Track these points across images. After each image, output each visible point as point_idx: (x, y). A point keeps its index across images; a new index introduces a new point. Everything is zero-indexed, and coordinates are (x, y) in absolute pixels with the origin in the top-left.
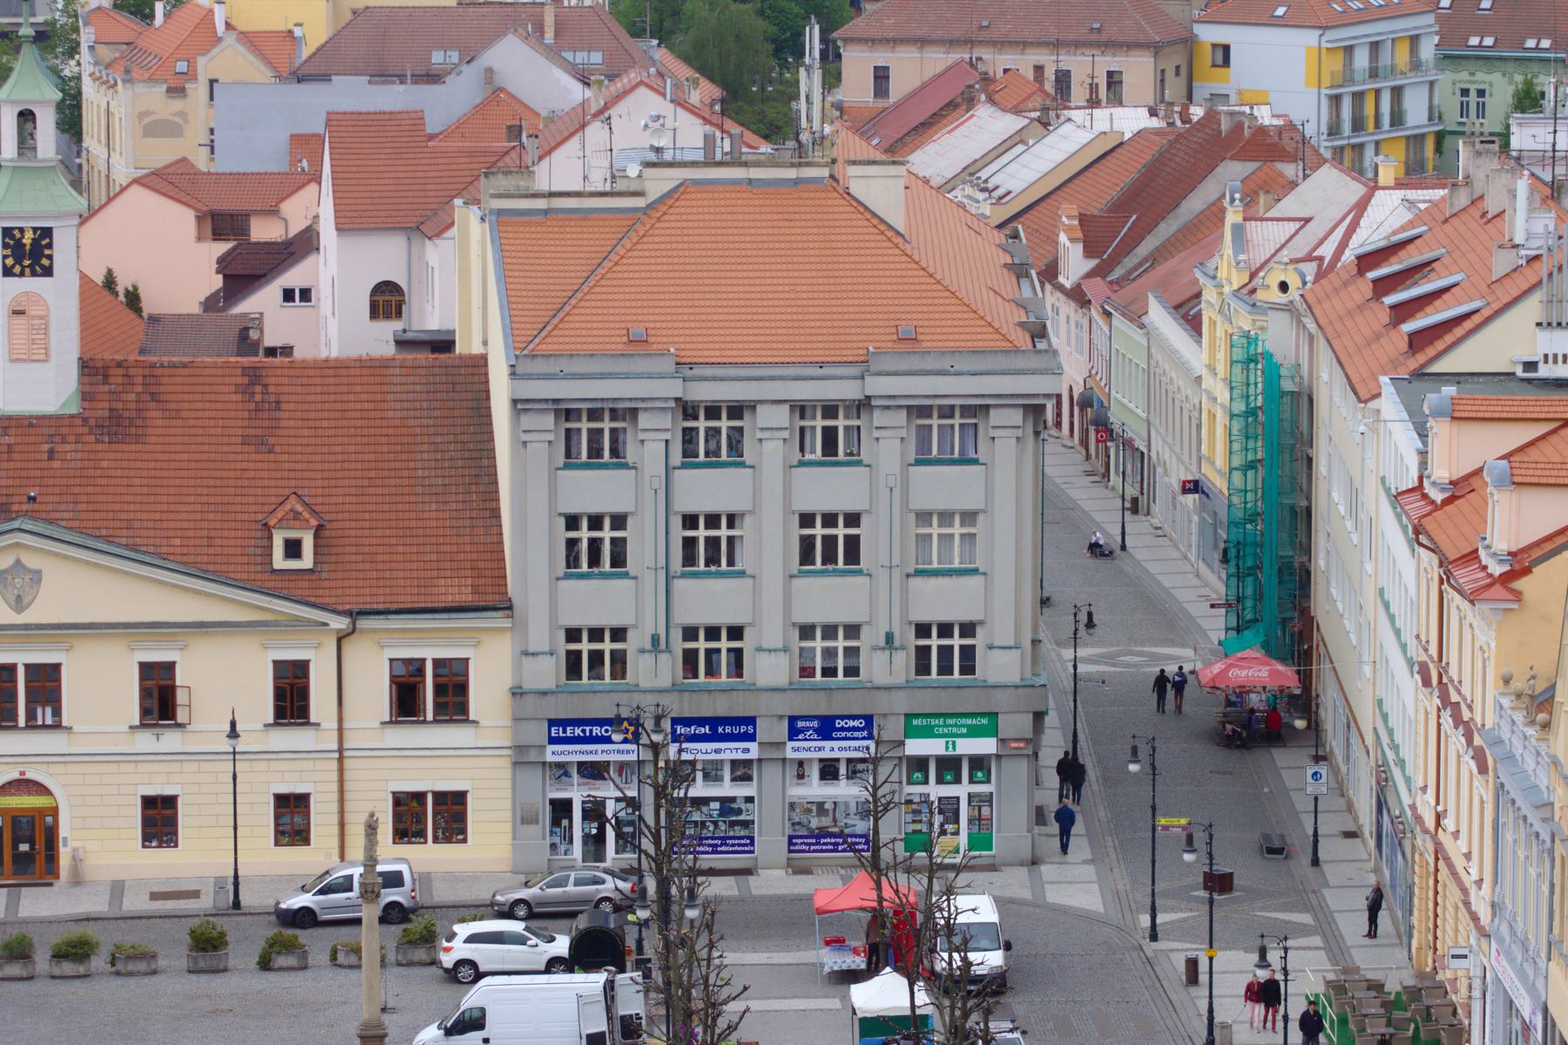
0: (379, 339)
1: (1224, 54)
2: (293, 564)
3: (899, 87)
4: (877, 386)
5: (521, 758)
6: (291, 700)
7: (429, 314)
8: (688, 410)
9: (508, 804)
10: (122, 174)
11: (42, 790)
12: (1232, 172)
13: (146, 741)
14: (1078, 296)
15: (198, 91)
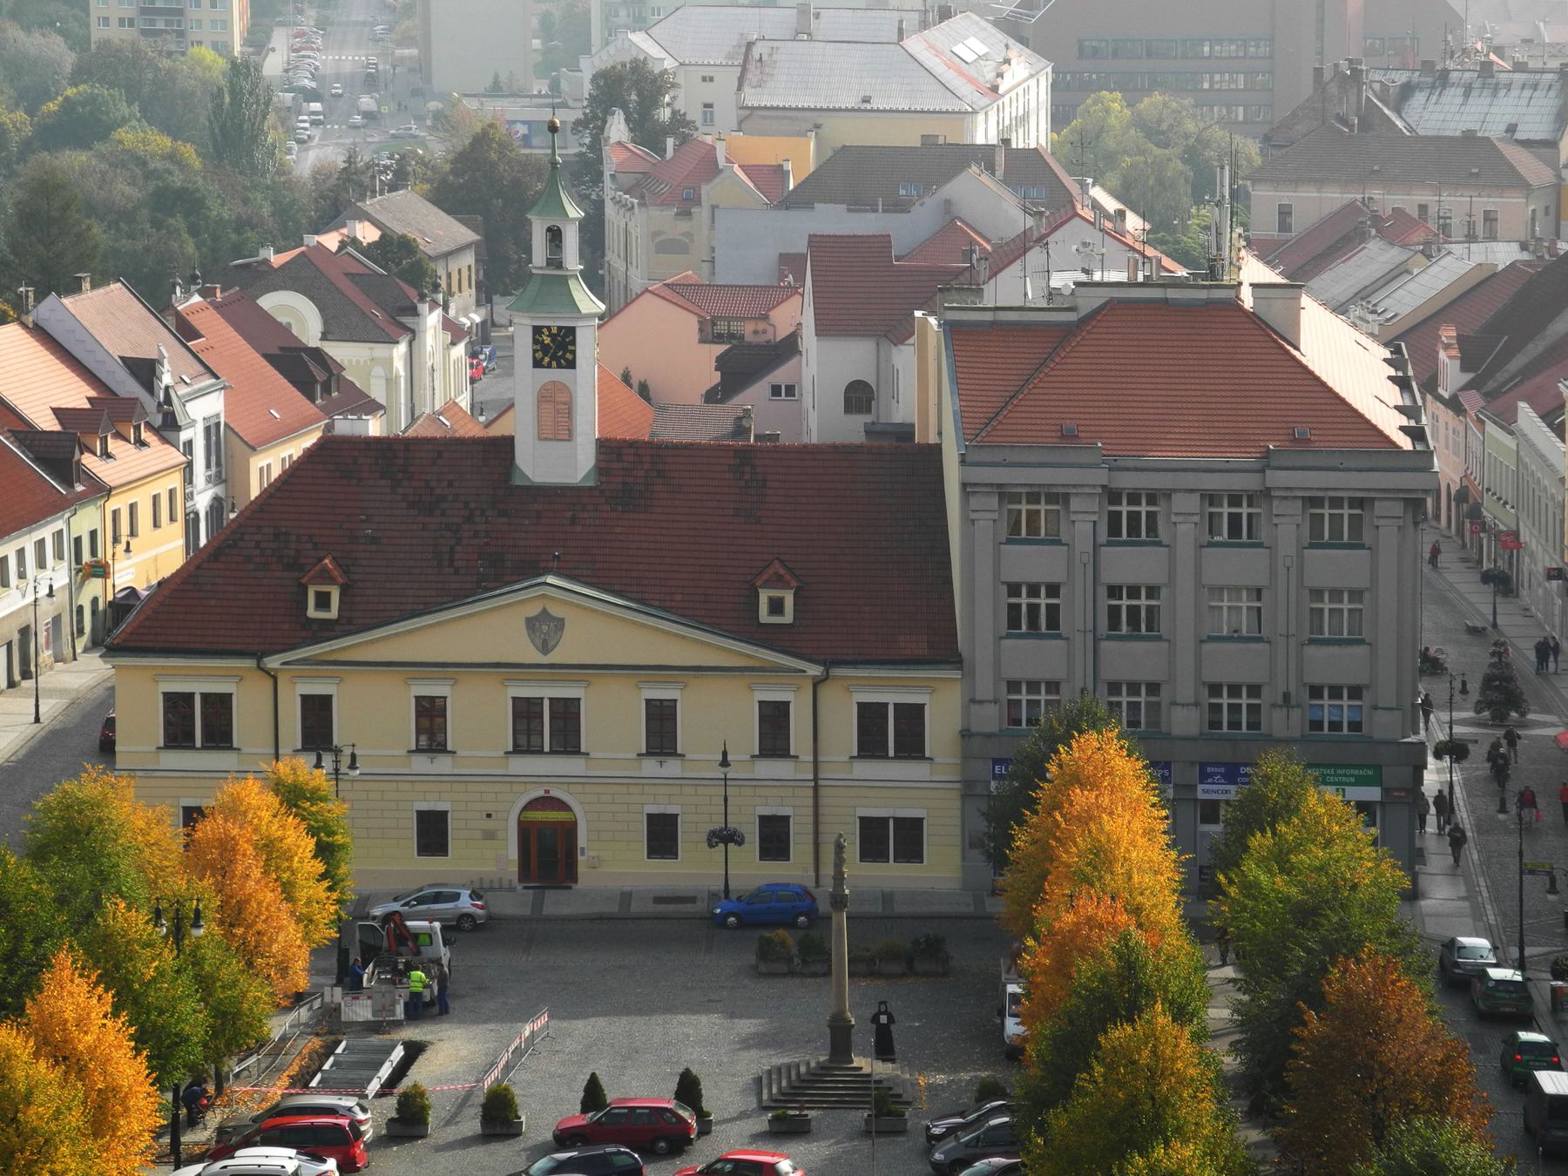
0: (852, 430)
3: (1299, 223)
4: (1277, 478)
6: (774, 719)
7: (903, 407)
8: (1114, 496)
9: (958, 831)
10: (637, 281)
11: (562, 805)
14: (1454, 405)
15: (702, 214)
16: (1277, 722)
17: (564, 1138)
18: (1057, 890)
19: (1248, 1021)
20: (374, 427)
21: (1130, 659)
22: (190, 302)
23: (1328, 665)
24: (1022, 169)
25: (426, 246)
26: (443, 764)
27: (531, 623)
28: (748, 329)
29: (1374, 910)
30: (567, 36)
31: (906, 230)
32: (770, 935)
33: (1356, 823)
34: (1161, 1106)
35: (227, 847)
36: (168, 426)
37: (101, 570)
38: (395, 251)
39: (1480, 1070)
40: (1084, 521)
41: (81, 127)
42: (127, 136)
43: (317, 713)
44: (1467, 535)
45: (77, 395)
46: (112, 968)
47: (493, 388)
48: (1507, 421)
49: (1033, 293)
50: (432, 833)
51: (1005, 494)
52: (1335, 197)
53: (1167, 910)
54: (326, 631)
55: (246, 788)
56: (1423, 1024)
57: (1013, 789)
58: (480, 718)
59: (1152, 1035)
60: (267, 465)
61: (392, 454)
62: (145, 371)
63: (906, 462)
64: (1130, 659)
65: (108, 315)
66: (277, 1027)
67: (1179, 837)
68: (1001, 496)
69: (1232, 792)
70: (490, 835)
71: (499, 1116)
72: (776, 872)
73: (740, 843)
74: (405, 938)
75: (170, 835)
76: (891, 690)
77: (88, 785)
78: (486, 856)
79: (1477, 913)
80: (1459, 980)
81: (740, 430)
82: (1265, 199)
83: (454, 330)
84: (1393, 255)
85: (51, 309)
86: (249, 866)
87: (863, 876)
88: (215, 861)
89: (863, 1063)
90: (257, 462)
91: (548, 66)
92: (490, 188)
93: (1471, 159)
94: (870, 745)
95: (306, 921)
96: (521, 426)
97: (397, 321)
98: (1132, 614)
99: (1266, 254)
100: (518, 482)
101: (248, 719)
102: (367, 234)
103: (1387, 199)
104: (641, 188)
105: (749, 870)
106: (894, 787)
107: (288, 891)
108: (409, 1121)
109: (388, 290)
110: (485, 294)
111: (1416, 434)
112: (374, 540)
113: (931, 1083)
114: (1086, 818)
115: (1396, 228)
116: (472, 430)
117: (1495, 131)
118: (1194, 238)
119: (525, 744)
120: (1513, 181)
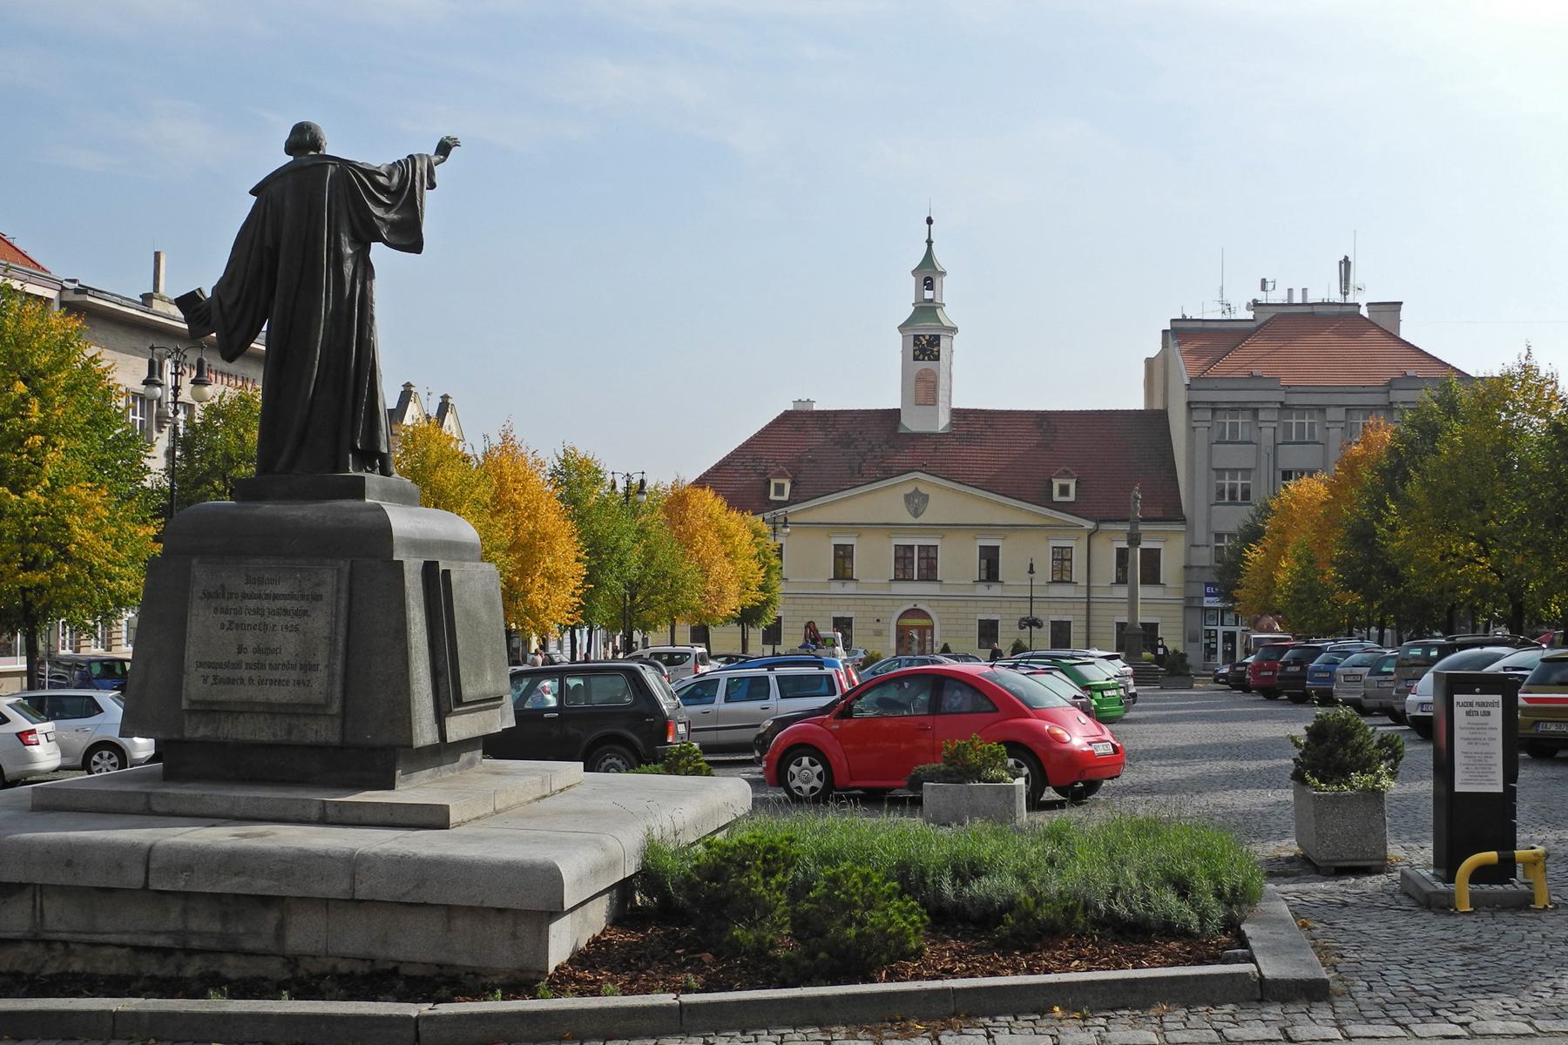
2: (1065, 482)
5: (1190, 604)
6: (1062, 558)
8: (1284, 407)
9: (1181, 631)
11: (925, 615)
13: (982, 590)
26: (850, 588)
27: (908, 498)
51: (1215, 408)
68: (1214, 410)
70: (878, 633)
73: (1040, 626)
100: (901, 431)
112: (811, 461)
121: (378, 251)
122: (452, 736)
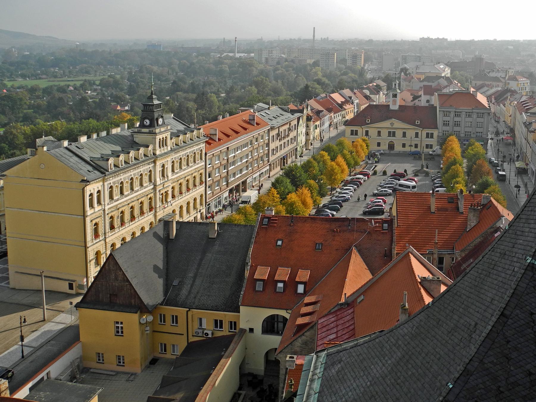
0: (427, 105)
1: (509, 83)
3: (477, 85)
4: (474, 111)
6: (417, 135)
7: (433, 102)
8: (456, 112)
10: (404, 89)
12: (509, 94)
13: (378, 137)
14: (494, 104)
15: (411, 83)
16: (472, 136)
17: (392, 176)
18: (447, 152)
19: (467, 166)
20: (375, 103)
21: (456, 129)
22: (355, 91)
23: (479, 130)
24: (447, 79)
25: (381, 85)
26: (380, 137)
28: (416, 94)
29: (482, 155)
30: (398, 65)
31: (434, 85)
32: (416, 156)
33: (481, 146)
34: (457, 174)
35: (357, 145)
36: (353, 103)
37: (345, 117)
38: (378, 86)
39: (492, 171)
40: (452, 114)
41: (345, 74)
42: (350, 75)
43: (367, 132)
44: (188, 197)
45: (343, 100)
46: (344, 157)
47: (387, 100)
48: (499, 106)
49: (448, 91)
50: (379, 144)
51: (444, 111)
52: (481, 82)
53: (459, 154)
54: (368, 124)
55: (359, 139)
56: (487, 167)
57: (443, 141)
58: (384, 133)
59: (457, 167)
60: (363, 107)
61: (376, 106)
62: (350, 98)
63: (433, 108)
64: (456, 129)
65: (347, 92)
66: (361, 163)
67: (461, 147)
69: (467, 143)
71: (385, 173)
72: (416, 149)
74: (375, 155)
75: (351, 144)
76: (430, 131)
77: (342, 139)
78: (384, 147)
79: (493, 155)
80: (491, 162)
81: (415, 104)
82: (474, 82)
83: (384, 94)
84: (488, 88)
85: (341, 91)
86: (359, 147)
87: (426, 150)
88: (356, 147)
89: (425, 169)
90: (362, 107)
91: (395, 68)
92: (388, 80)
93: (496, 79)
94: (427, 136)
95: (365, 153)
96: (391, 104)
97: (378, 93)
98: (457, 124)
99: (474, 88)
101: (359, 133)
102: (375, 84)
103: (487, 83)
104: (405, 80)
105: (413, 149)
106: (430, 141)
107: (363, 150)
108: (375, 173)
109: (377, 90)
110: (387, 90)
111: (489, 107)
113: (432, 171)
114: (451, 145)
115: (488, 86)
116: (385, 104)
117: (499, 76)
118: (466, 86)
119: (389, 136)
120: (500, 81)
121: (127, 241)
122: (279, 323)
